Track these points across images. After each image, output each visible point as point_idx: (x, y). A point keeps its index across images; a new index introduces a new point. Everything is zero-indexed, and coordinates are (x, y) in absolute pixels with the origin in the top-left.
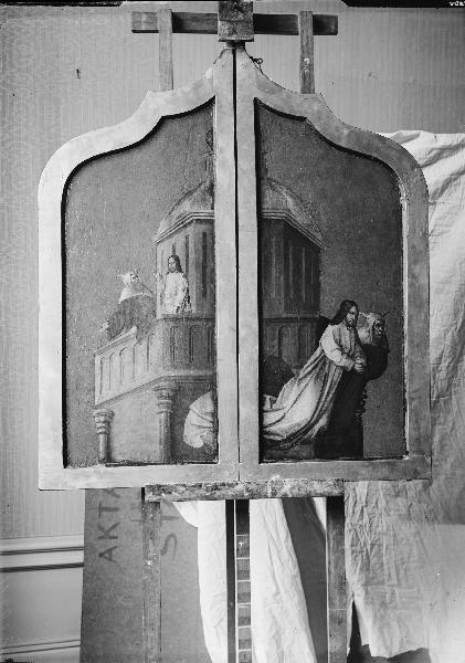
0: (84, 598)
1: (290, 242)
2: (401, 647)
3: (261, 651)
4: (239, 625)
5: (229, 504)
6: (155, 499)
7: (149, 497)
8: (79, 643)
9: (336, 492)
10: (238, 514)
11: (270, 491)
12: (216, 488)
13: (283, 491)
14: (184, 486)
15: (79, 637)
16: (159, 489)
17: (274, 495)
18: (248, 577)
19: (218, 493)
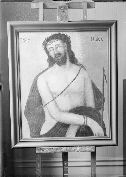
9: (93, 150)
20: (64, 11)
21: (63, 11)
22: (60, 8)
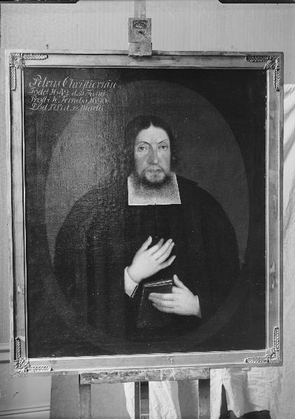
0: (52, 385)
1: (174, 257)
2: (136, 13)
3: (153, 413)
4: (142, 399)
5: (136, 384)
6: (87, 382)
7: (84, 381)
8: (49, 408)
9: (205, 377)
10: (142, 389)
11: (162, 376)
12: (127, 374)
13: (171, 376)
14: (107, 373)
15: (49, 404)
16: (91, 376)
17: (164, 379)
18: (148, 413)
19: (128, 378)
20: (143, 30)
21: (140, 32)
22: (134, 26)
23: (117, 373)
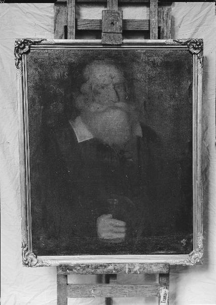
23: (89, 266)
